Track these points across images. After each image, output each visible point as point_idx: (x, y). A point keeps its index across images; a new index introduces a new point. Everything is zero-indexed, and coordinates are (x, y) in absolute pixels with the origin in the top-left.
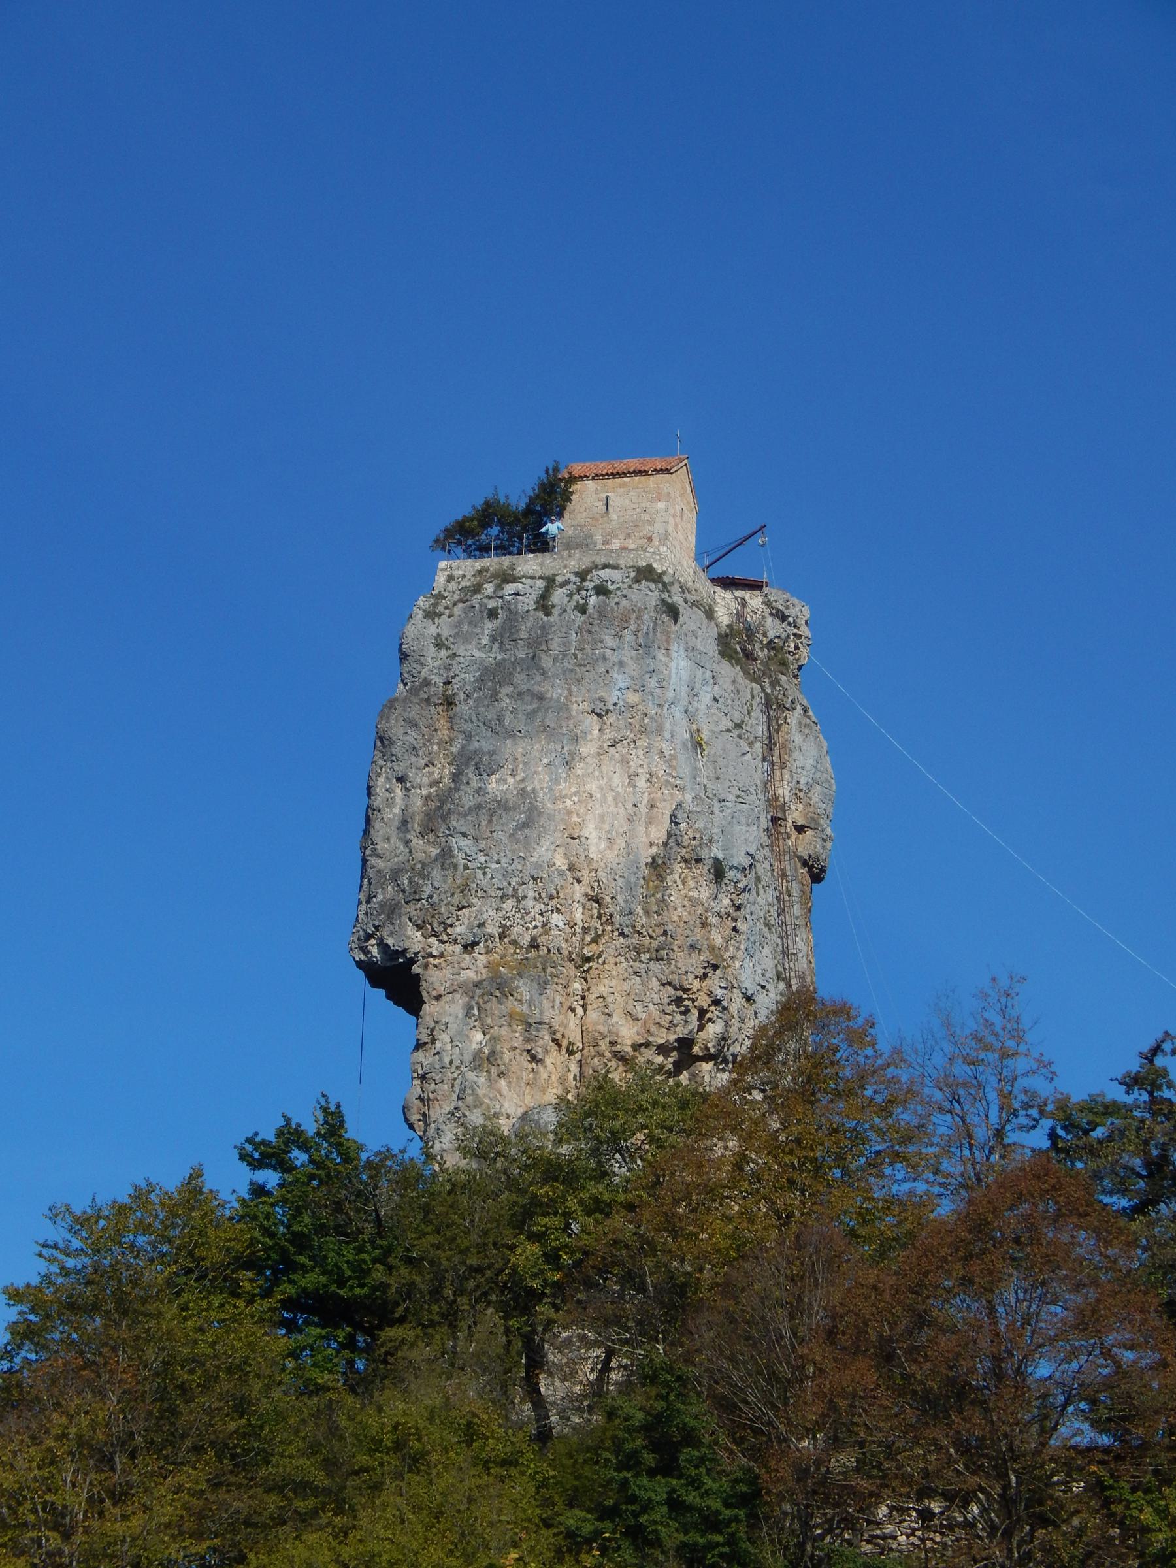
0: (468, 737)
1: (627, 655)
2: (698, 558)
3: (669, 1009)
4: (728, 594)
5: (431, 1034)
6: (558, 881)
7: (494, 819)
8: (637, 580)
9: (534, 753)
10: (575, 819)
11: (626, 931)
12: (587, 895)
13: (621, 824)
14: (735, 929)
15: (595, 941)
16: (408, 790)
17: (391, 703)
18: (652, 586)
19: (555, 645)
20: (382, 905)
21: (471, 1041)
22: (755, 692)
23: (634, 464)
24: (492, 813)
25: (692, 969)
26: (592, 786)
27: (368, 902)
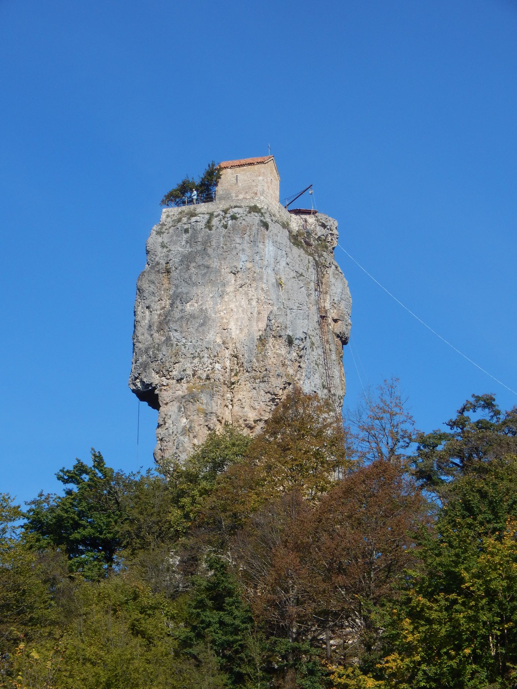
0: (177, 287)
1: (246, 246)
2: (281, 201)
4: (298, 217)
13: (246, 322)
17: (143, 274)
18: (256, 214)
19: (214, 243)
20: (141, 364)
22: (310, 260)
23: (249, 160)
24: (188, 320)
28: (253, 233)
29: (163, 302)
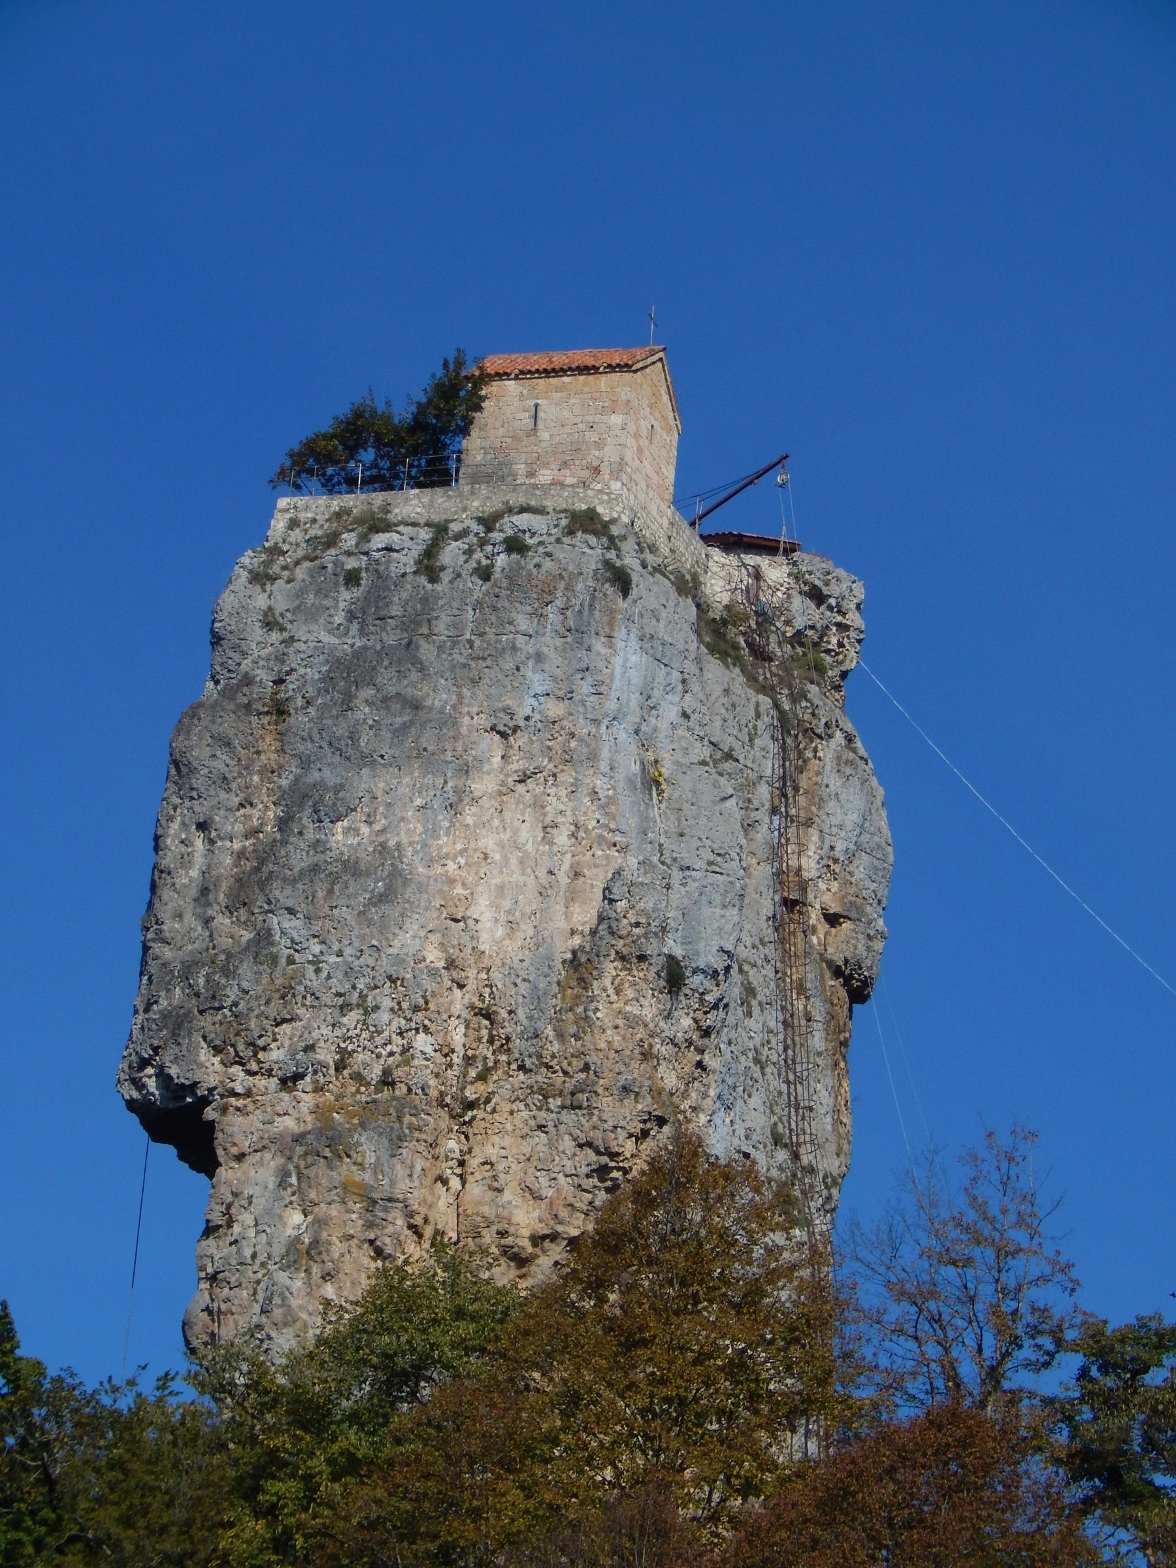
0: (306, 763)
1: (549, 643)
2: (680, 501)
3: (588, 1183)
4: (732, 560)
5: (227, 1212)
6: (429, 985)
7: (337, 888)
8: (571, 532)
9: (402, 790)
10: (459, 890)
11: (528, 1063)
12: (472, 1007)
13: (529, 900)
14: (700, 1065)
15: (482, 1077)
16: (212, 842)
17: (194, 712)
18: (593, 540)
19: (442, 627)
20: (165, 1015)
21: (284, 1225)
22: (762, 709)
23: (582, 357)
24: (334, 879)
25: (623, 1123)
26: (488, 842)
27: (146, 1010)
28: (576, 603)
29: (256, 813)
